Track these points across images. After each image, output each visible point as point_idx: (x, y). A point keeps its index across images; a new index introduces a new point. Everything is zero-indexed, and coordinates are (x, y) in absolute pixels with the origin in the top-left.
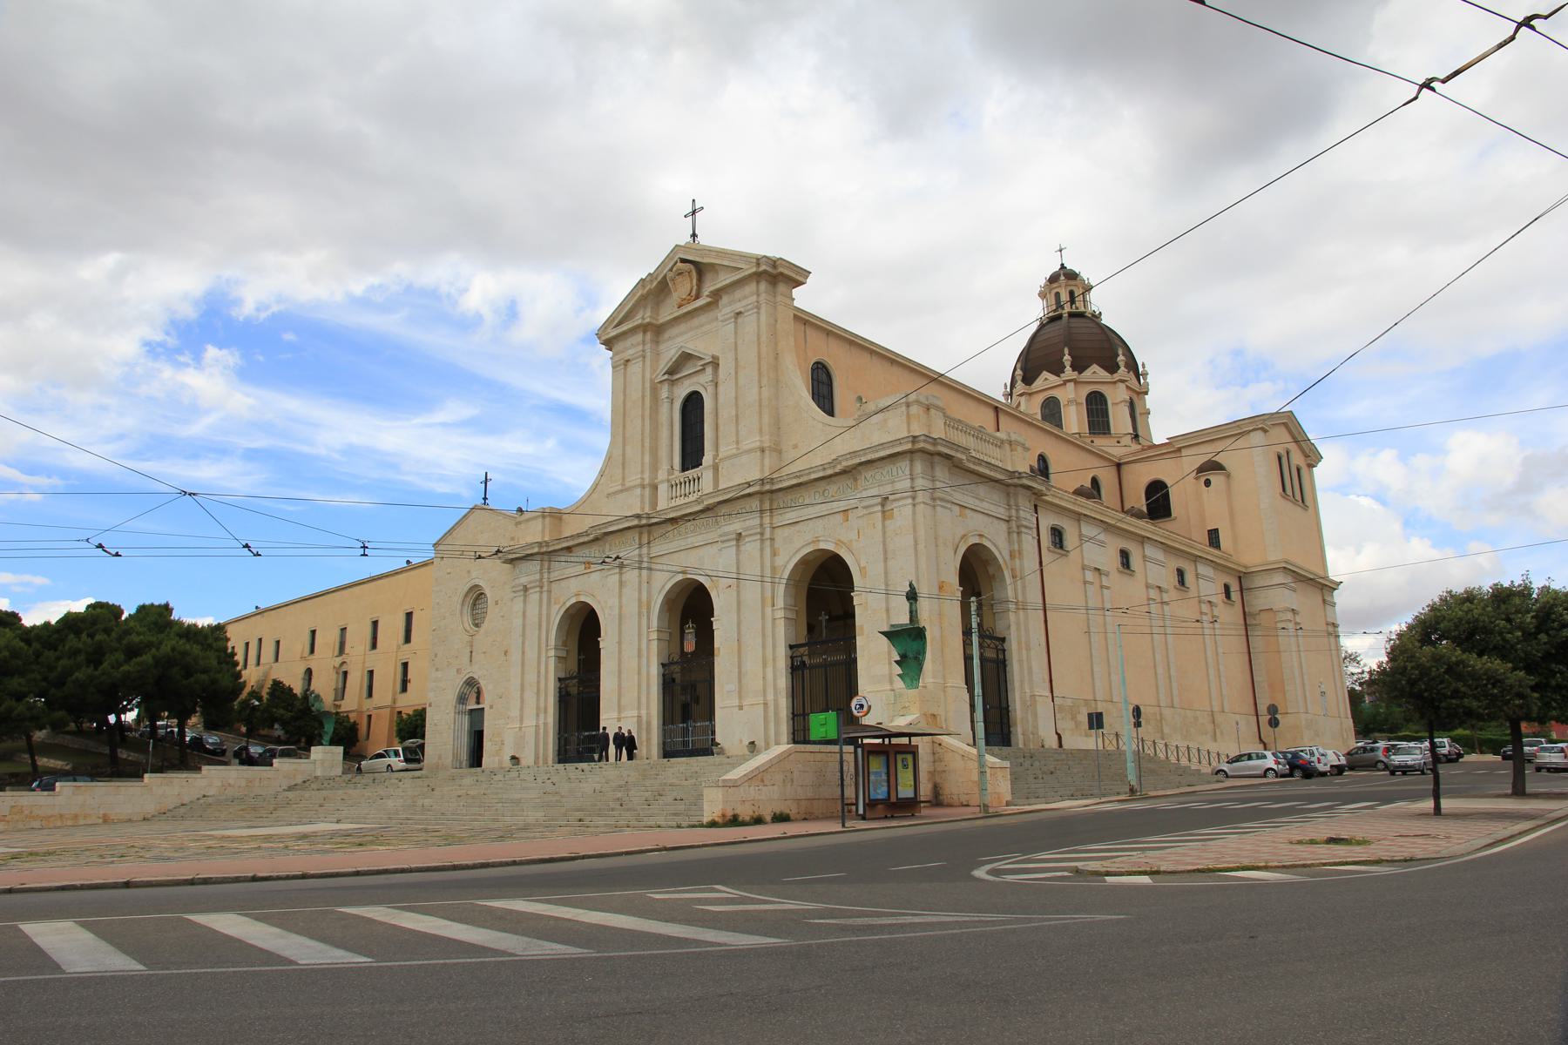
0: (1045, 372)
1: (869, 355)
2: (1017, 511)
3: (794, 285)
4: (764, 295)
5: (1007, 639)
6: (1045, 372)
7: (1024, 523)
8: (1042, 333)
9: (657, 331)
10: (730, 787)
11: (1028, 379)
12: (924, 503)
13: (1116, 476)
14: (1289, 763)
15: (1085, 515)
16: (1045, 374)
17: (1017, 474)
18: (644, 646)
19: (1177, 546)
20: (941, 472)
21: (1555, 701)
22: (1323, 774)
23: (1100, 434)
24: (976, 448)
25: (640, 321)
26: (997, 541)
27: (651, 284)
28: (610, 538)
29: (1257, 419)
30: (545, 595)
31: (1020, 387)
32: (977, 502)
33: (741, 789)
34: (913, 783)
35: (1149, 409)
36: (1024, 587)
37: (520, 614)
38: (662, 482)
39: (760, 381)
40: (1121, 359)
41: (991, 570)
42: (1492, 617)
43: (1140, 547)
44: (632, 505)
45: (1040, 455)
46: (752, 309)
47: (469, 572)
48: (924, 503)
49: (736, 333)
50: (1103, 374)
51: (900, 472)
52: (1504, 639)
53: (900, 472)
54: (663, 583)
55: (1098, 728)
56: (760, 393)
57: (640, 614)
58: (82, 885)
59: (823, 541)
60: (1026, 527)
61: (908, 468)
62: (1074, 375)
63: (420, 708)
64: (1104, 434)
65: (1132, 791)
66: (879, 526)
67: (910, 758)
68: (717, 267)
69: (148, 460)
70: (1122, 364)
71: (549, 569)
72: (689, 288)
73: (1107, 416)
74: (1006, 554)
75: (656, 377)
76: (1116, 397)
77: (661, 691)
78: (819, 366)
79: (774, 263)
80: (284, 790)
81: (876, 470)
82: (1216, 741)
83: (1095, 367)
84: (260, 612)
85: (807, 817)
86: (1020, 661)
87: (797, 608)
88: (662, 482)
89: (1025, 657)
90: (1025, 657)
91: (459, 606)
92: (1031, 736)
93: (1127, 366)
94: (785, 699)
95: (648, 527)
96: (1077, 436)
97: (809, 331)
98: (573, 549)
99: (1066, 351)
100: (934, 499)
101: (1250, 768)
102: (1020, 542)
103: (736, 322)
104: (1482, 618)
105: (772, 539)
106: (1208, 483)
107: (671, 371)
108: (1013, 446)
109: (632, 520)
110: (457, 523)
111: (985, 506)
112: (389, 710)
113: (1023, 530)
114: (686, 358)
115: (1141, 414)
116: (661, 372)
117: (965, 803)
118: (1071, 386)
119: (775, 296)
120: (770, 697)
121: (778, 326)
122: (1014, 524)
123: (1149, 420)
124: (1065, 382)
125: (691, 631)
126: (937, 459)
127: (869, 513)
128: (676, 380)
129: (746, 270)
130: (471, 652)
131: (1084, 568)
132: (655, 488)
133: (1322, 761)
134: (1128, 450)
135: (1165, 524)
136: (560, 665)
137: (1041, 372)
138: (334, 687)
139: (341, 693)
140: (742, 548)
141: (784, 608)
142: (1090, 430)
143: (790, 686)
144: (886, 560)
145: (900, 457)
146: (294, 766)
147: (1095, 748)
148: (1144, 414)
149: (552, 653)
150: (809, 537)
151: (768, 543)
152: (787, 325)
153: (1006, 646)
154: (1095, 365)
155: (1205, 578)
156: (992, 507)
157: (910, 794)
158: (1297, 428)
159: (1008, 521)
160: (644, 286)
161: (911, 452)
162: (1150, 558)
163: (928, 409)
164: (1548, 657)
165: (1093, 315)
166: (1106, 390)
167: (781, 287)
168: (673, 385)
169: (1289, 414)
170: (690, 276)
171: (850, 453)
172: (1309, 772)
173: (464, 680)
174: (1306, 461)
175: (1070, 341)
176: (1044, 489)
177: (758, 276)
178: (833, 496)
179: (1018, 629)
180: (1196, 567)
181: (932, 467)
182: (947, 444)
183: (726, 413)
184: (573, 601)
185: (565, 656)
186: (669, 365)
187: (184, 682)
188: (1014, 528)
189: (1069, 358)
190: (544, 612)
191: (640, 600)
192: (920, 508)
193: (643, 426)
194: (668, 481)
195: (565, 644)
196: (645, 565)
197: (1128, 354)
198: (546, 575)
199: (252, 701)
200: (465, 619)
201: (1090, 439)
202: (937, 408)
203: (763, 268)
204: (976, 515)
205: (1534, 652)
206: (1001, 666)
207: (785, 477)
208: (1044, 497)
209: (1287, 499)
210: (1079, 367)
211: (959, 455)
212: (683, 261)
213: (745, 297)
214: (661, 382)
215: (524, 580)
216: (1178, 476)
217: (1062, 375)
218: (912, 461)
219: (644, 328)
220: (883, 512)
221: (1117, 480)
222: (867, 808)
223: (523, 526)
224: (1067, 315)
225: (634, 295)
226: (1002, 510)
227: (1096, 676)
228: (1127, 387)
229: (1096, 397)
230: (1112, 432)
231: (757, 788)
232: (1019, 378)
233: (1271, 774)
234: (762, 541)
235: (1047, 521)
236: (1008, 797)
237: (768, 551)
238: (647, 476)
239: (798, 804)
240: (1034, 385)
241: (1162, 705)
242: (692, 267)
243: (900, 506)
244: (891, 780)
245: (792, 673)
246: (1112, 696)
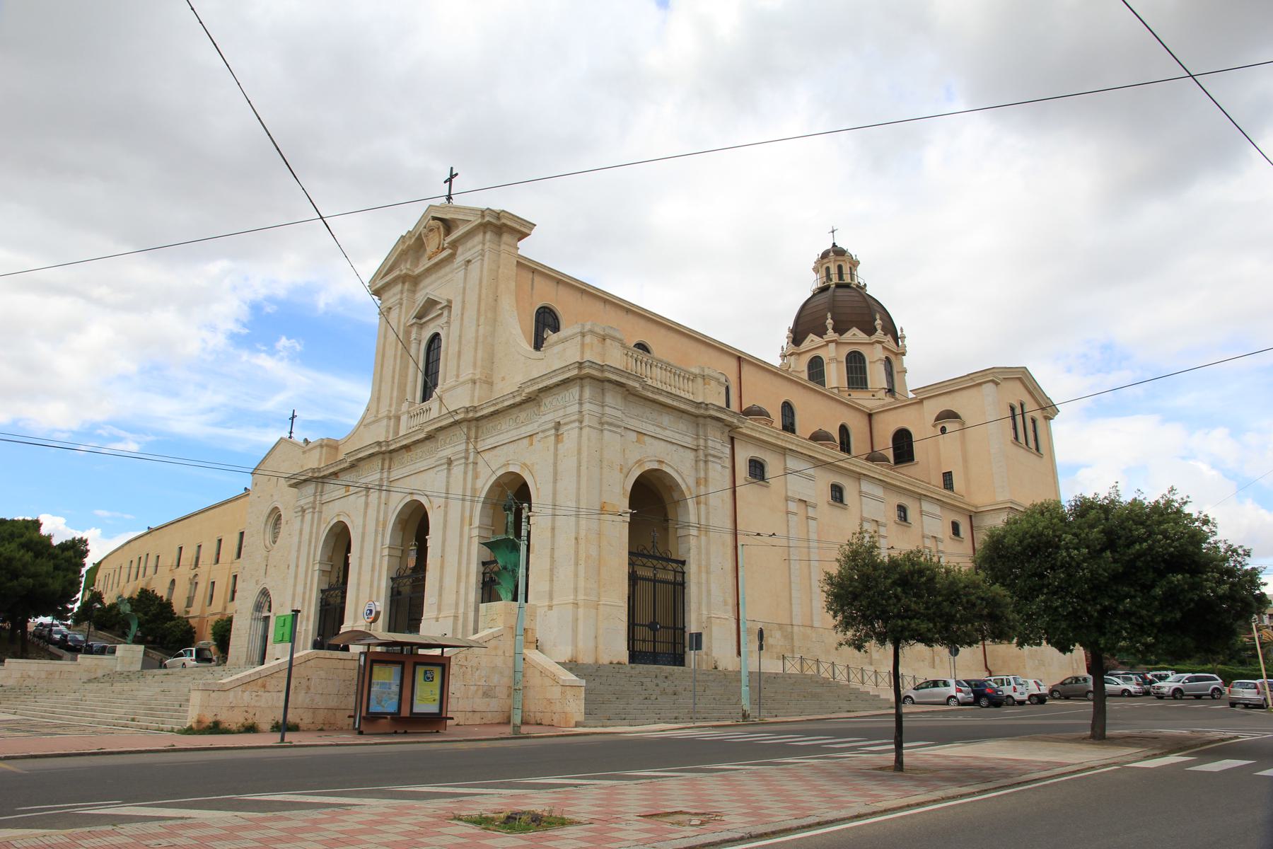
0: (811, 335)
1: (580, 294)
2: (706, 440)
3: (520, 236)
4: (488, 244)
5: (686, 563)
6: (811, 335)
7: (712, 452)
8: (813, 300)
9: (414, 281)
10: (214, 691)
12: (589, 426)
13: (868, 425)
14: (973, 691)
15: (790, 450)
16: (811, 336)
17: (703, 405)
18: (377, 562)
19: (898, 484)
20: (612, 398)
21: (1125, 629)
22: (1021, 703)
23: (857, 388)
25: (398, 273)
26: (680, 468)
27: (411, 241)
28: (362, 463)
29: (988, 372)
30: (316, 515)
32: (658, 430)
33: (231, 694)
34: (437, 697)
36: (708, 513)
37: (298, 532)
38: (404, 413)
39: (478, 320)
40: (878, 322)
41: (676, 496)
43: (857, 484)
44: (380, 433)
45: (784, 403)
46: (478, 256)
47: (272, 496)
48: (589, 426)
49: (465, 279)
51: (571, 397)
52: (1069, 555)
53: (571, 397)
54: (397, 502)
55: (696, 649)
56: (477, 331)
57: (376, 531)
58: (6, 757)
59: (513, 464)
60: (714, 456)
61: (578, 394)
62: (835, 336)
63: (230, 615)
65: (745, 716)
66: (552, 448)
67: (437, 672)
68: (458, 222)
69: (231, 428)
70: (879, 327)
71: (322, 492)
72: (437, 243)
73: (865, 373)
74: (691, 482)
75: (408, 320)
76: (874, 357)
77: (389, 603)
78: (546, 310)
79: (498, 215)
80: (84, 682)
81: (554, 397)
82: (934, 668)
83: (855, 330)
84: (151, 531)
85: (325, 728)
86: (699, 583)
87: (493, 528)
88: (404, 413)
89: (703, 581)
90: (703, 581)
91: (263, 525)
92: (705, 657)
94: (473, 613)
95: (388, 454)
97: (537, 279)
98: (339, 474)
99: (829, 315)
100: (602, 424)
101: (933, 695)
102: (706, 470)
103: (466, 269)
104: (1046, 532)
105: (475, 463)
106: (943, 430)
107: (420, 316)
108: (707, 380)
109: (374, 448)
110: (268, 454)
111: (668, 434)
113: (710, 458)
114: (431, 303)
115: (898, 372)
116: (411, 316)
117: (539, 722)
118: (832, 346)
119: (500, 246)
120: (461, 610)
121: (500, 271)
122: (701, 453)
123: (906, 378)
125: (413, 548)
126: (607, 385)
127: (546, 437)
128: (424, 323)
129: (474, 221)
130: (267, 565)
131: (787, 499)
132: (398, 418)
133: (1018, 690)
134: (881, 402)
135: (906, 469)
136: (324, 578)
138: (187, 596)
139: (189, 604)
140: (452, 472)
141: (479, 527)
144: (555, 481)
145: (571, 383)
146: (96, 662)
147: (758, 671)
148: (901, 372)
149: (317, 567)
150: (503, 461)
151: (471, 466)
152: (509, 269)
153: (686, 568)
155: (928, 514)
157: (433, 708)
159: (696, 450)
160: (404, 242)
161: (580, 378)
162: (866, 493)
163: (604, 340)
164: (1116, 578)
165: (858, 286)
167: (506, 238)
168: (421, 328)
170: (439, 232)
171: (530, 380)
172: (997, 701)
173: (259, 590)
175: (833, 307)
176: (735, 421)
177: (484, 227)
178: (522, 423)
179: (699, 553)
180: (921, 504)
181: (603, 394)
182: (616, 371)
183: (453, 349)
184: (335, 520)
185: (330, 570)
186: (417, 311)
187: (9, 584)
188: (702, 457)
189: (831, 321)
190: (314, 531)
191: (377, 519)
192: (586, 431)
193: (395, 365)
194: (409, 412)
195: (330, 559)
196: (384, 488)
197: (887, 319)
198: (318, 498)
199: (95, 604)
200: (267, 536)
201: (848, 393)
202: (614, 338)
203: (487, 219)
204: (656, 442)
205: (1101, 571)
206: (679, 588)
207: (485, 406)
209: (1020, 447)
210: (840, 329)
211: (631, 383)
212: (434, 218)
213: (474, 247)
214: (412, 325)
215: (302, 502)
216: (920, 424)
218: (582, 387)
219: (403, 279)
220: (557, 436)
221: (868, 429)
222: (362, 721)
223: (307, 455)
224: (834, 286)
225: (397, 250)
226: (689, 440)
227: (794, 601)
228: (884, 348)
229: (855, 356)
231: (254, 694)
233: (953, 702)
234: (466, 464)
235: (744, 454)
236: (580, 717)
237: (470, 474)
238: (393, 409)
239: (314, 713)
241: (816, 624)
242: (439, 223)
243: (568, 430)
244: (406, 690)
245: (482, 588)
246: (812, 621)
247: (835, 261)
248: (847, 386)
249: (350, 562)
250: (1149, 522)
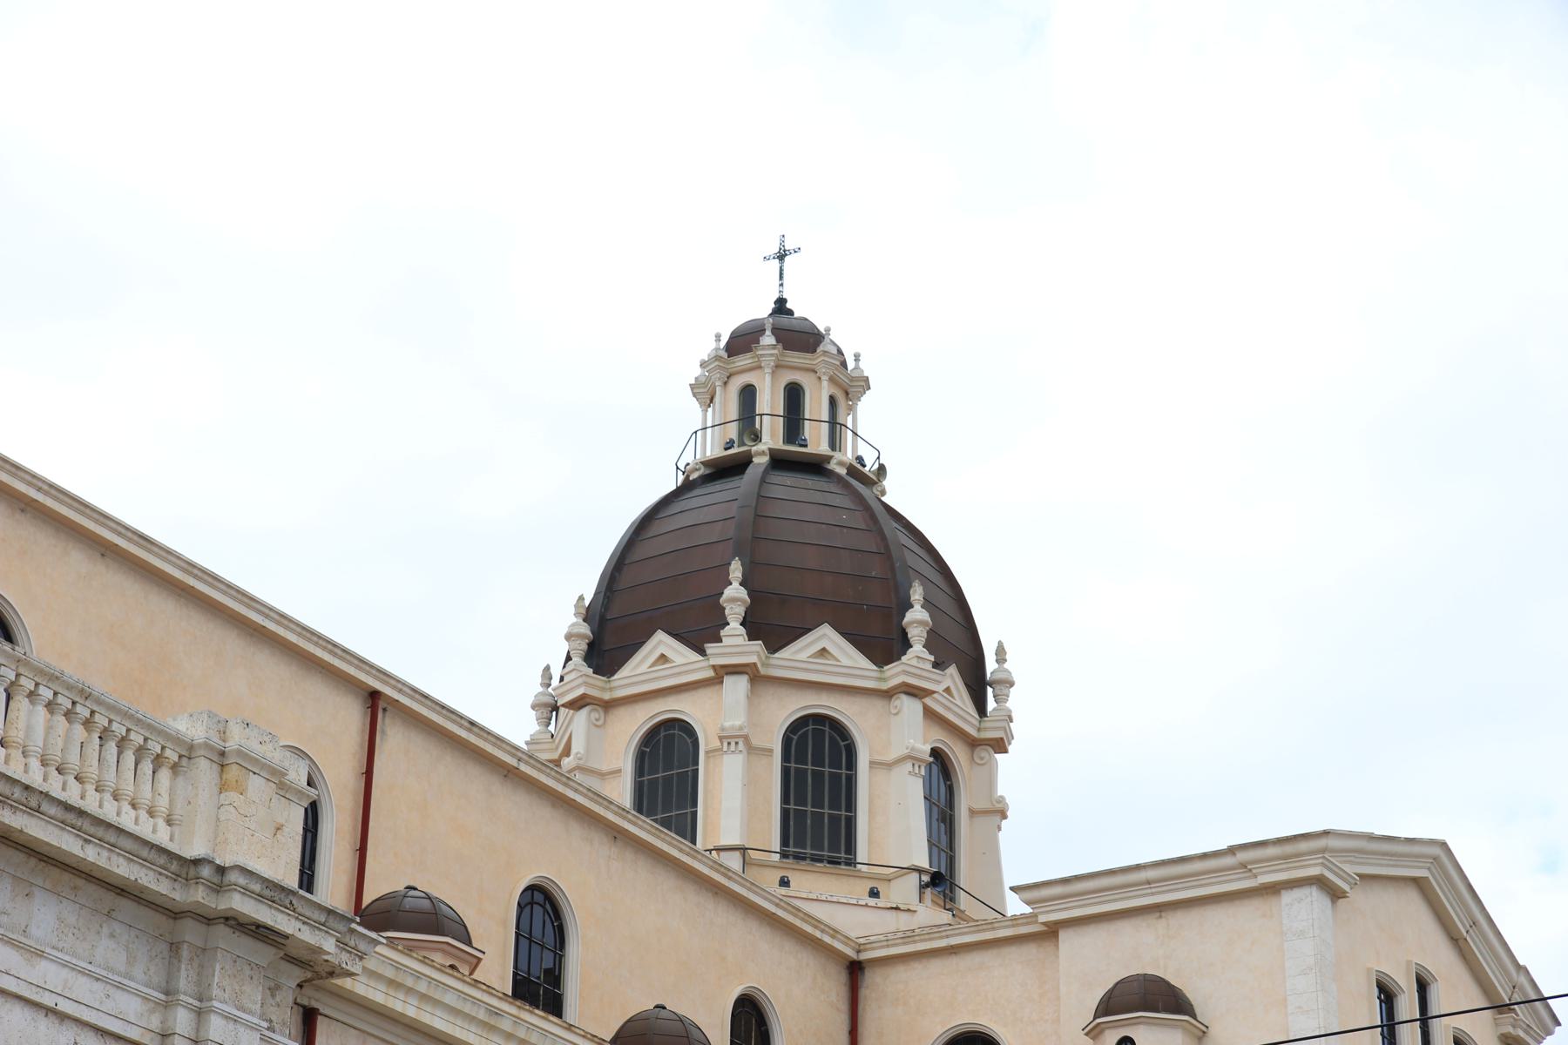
0: (826, 629)
2: (200, 1014)
13: (844, 1006)
16: (661, 642)
17: (206, 872)
24: (56, 754)
29: (1303, 846)
35: (1001, 800)
40: (917, 617)
50: (849, 661)
62: (753, 652)
70: (917, 635)
73: (851, 804)
83: (826, 636)
93: (934, 642)
96: (733, 861)
99: (736, 570)
108: (233, 772)
111: (47, 978)
115: (973, 813)
118: (737, 687)
124: (723, 672)
134: (902, 922)
137: (654, 632)
142: (785, 841)
154: (826, 629)
156: (83, 988)
165: (855, 471)
166: (688, 708)
169: (1437, 851)
174: (1496, 1024)
176: (329, 945)
189: (743, 593)
208: (338, 981)
217: (711, 648)
224: (765, 459)
226: (131, 1006)
228: (929, 713)
229: (818, 735)
230: (862, 855)
240: (616, 677)
248: (776, 845)
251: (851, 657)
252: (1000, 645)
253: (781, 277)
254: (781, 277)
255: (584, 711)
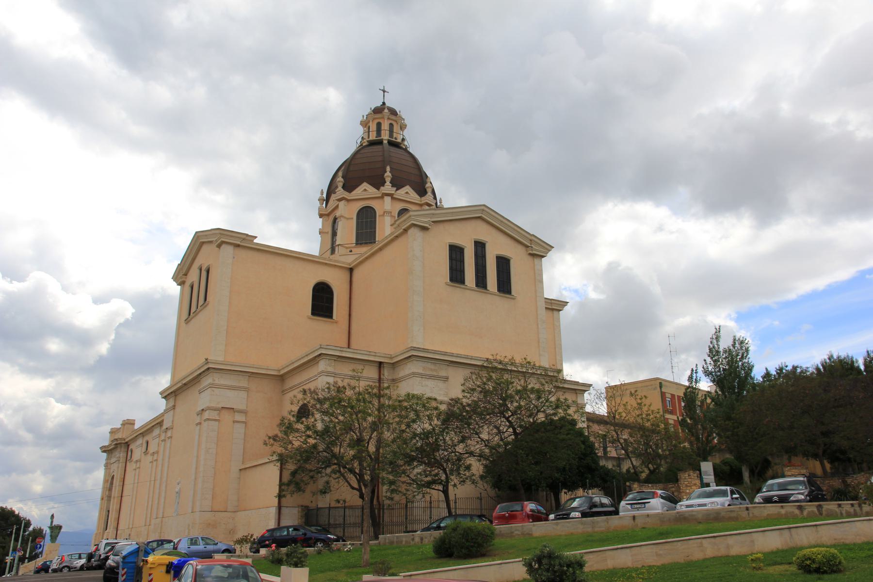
11: (349, 186)
31: (340, 192)
42: (415, 492)
62: (392, 190)
64: (371, 243)
83: (407, 189)
99: (388, 169)
112: (78, 555)
143: (277, 518)
158: (232, 236)
166: (373, 204)
210: (398, 184)
221: (347, 286)
232: (340, 185)
247: (374, 119)
248: (354, 241)
249: (104, 304)
250: (344, 432)
251: (414, 195)
252: (441, 199)
253: (384, 97)
254: (384, 97)
255: (343, 201)
